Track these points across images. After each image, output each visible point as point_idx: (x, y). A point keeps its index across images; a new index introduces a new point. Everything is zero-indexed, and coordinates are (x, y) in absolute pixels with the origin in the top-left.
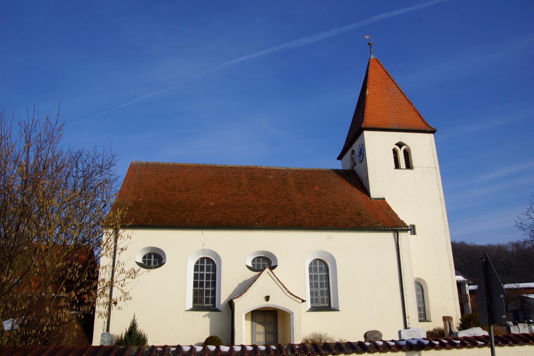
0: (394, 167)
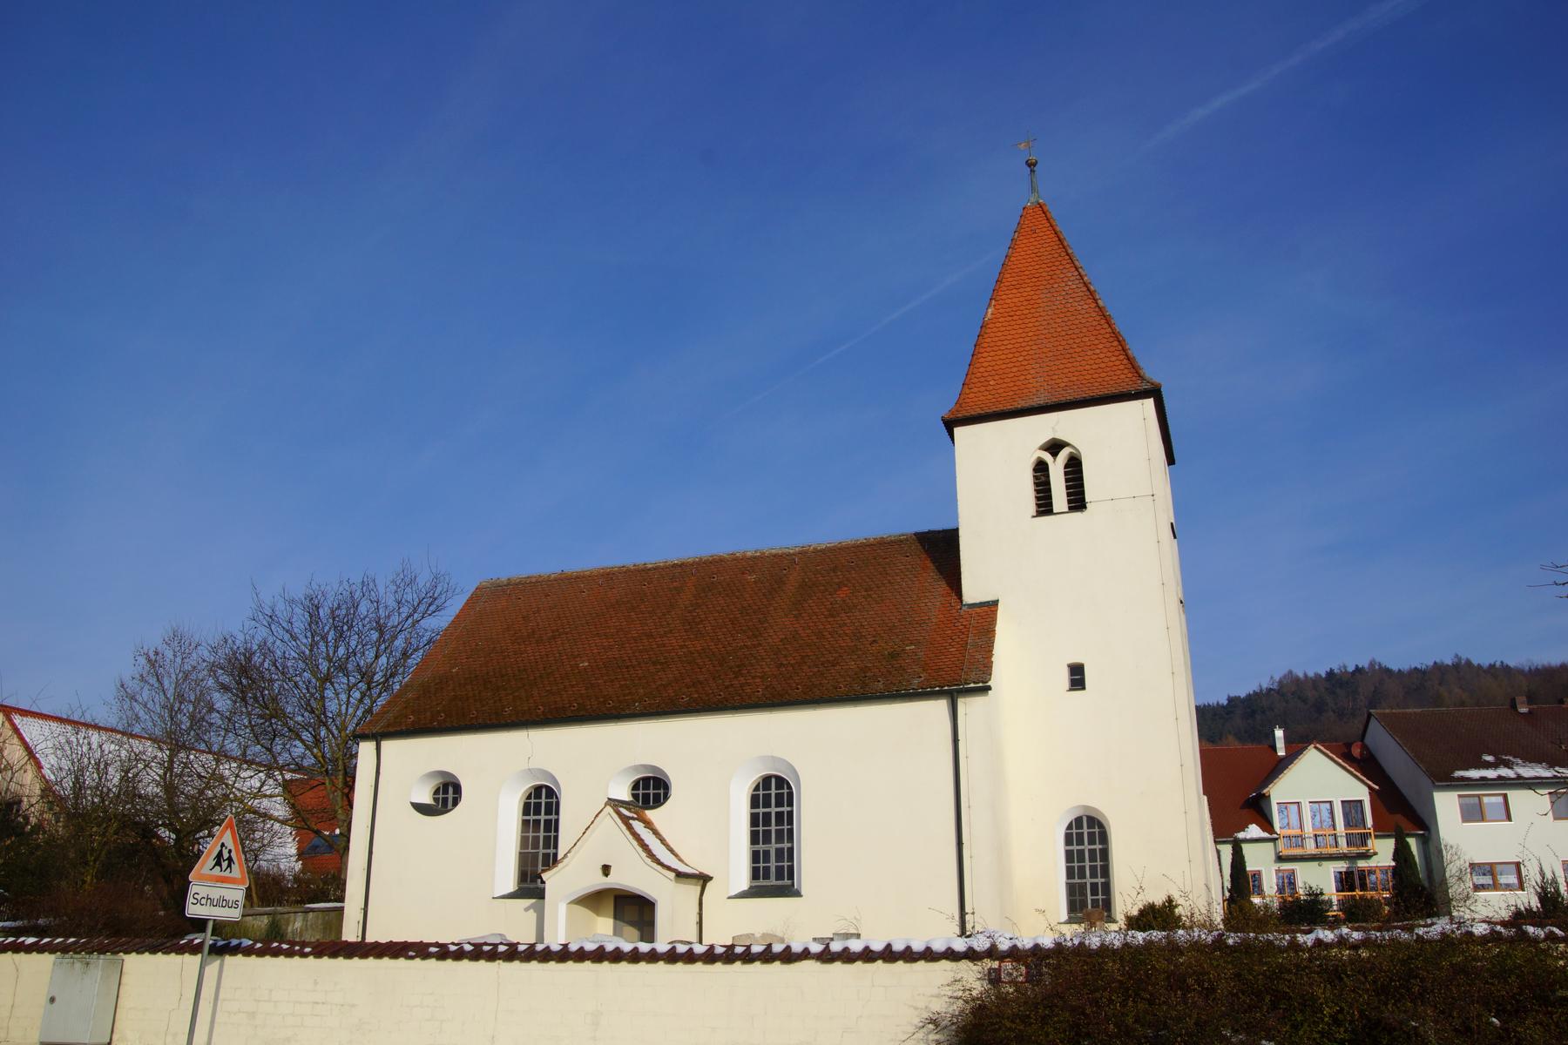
0: (1032, 509)
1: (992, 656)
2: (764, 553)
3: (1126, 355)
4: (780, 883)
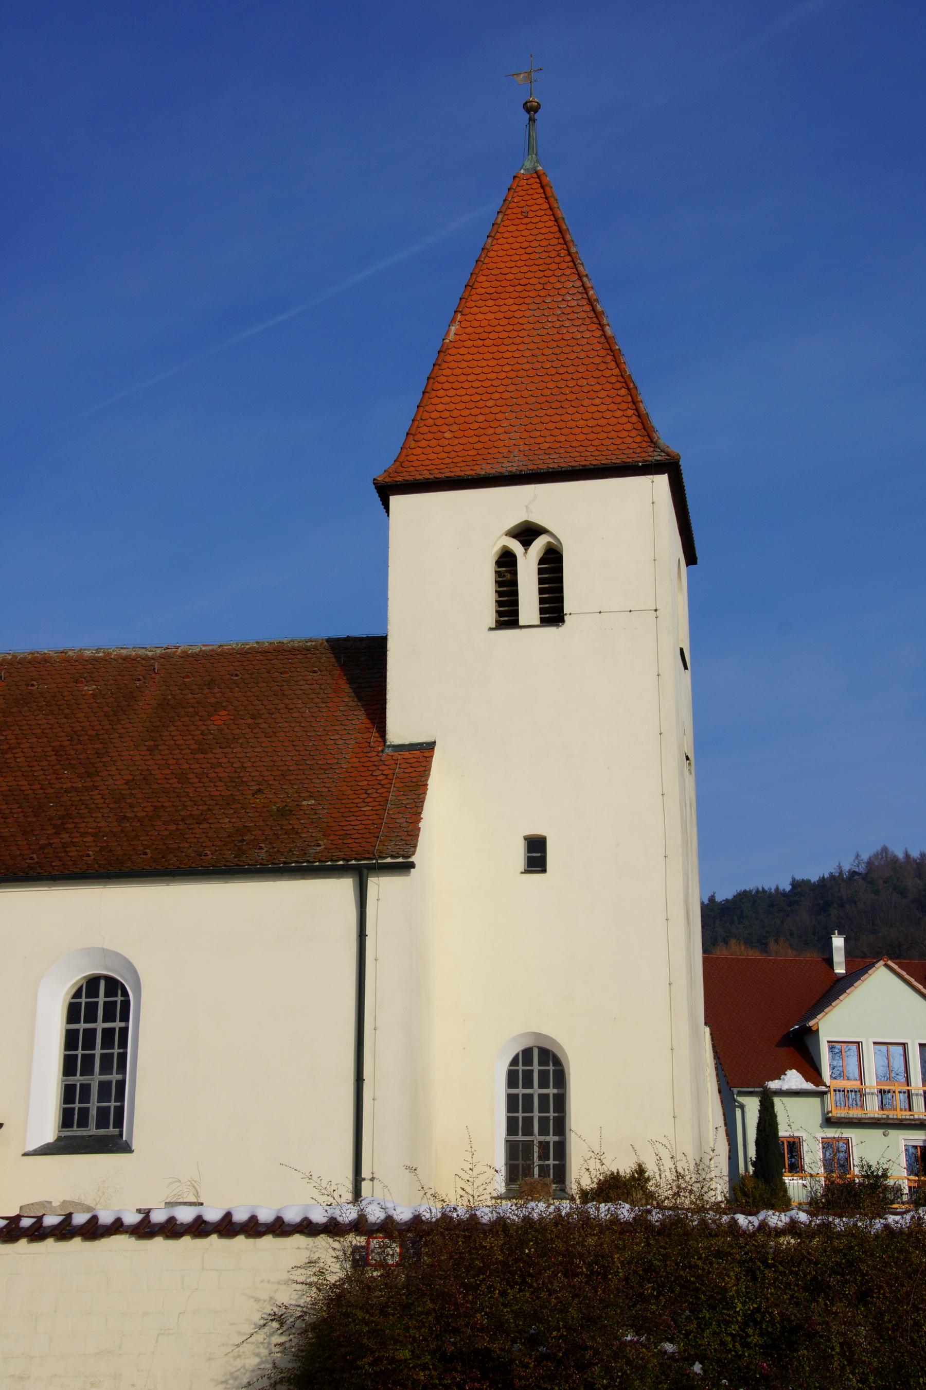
0: (490, 617)
1: (419, 819)
2: (110, 654)
3: (637, 410)
4: (102, 1132)
